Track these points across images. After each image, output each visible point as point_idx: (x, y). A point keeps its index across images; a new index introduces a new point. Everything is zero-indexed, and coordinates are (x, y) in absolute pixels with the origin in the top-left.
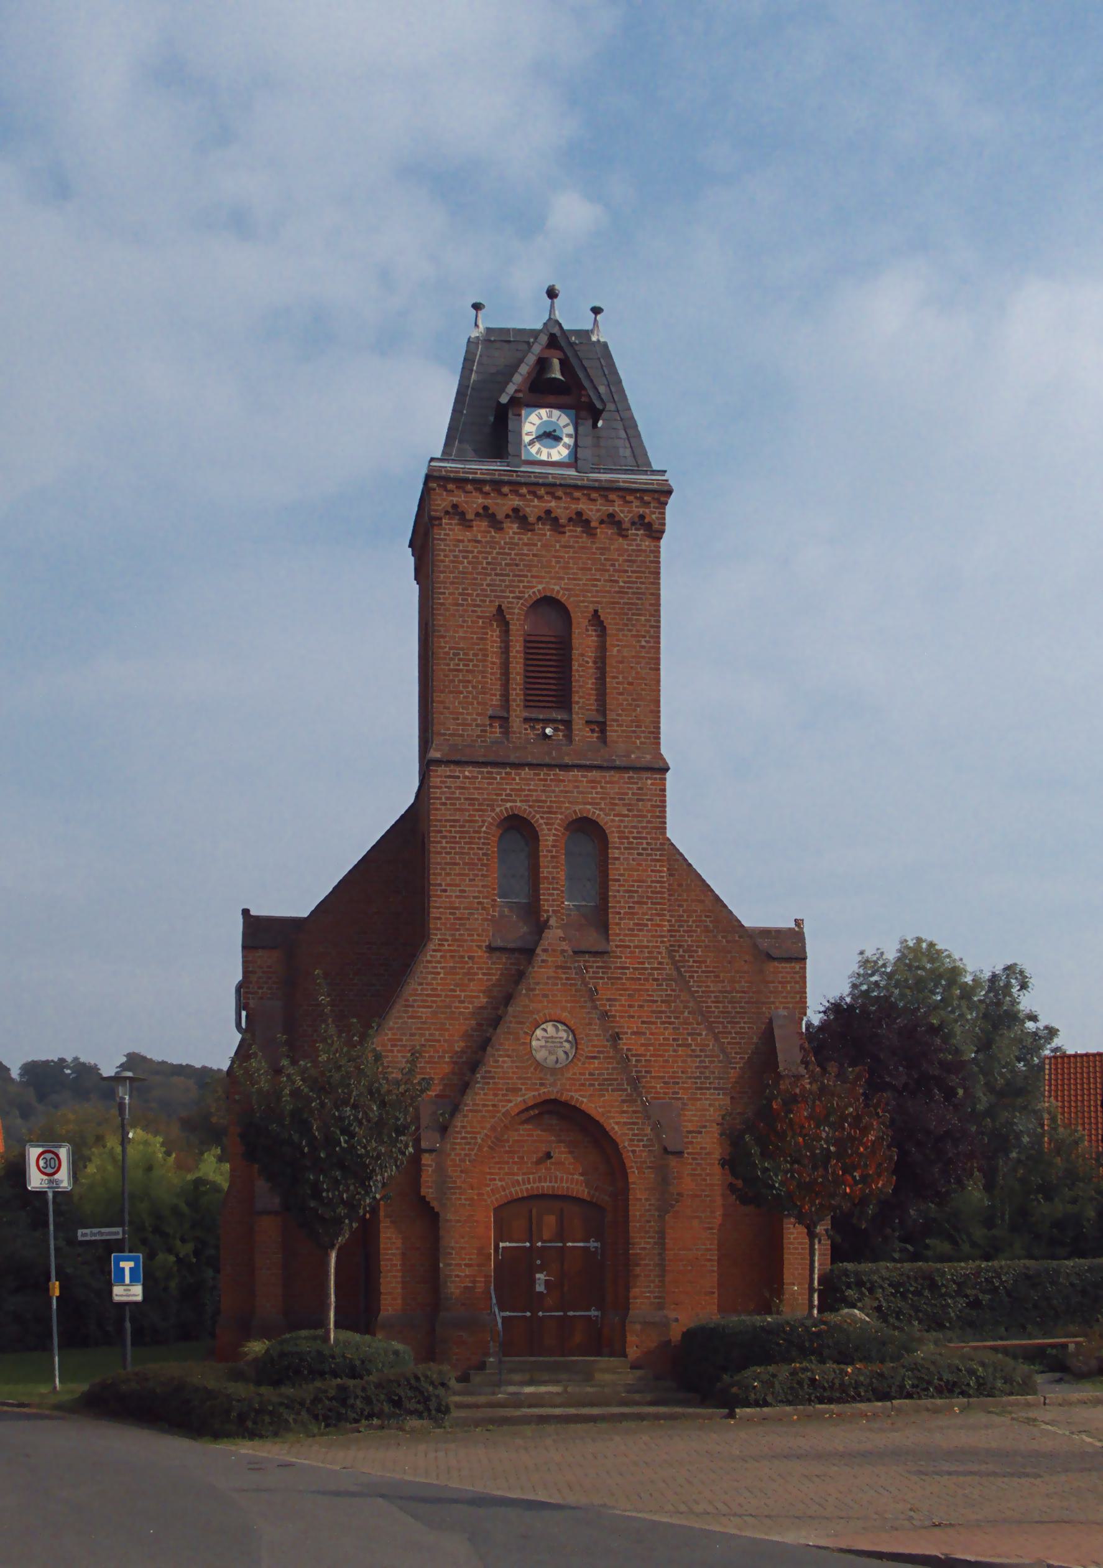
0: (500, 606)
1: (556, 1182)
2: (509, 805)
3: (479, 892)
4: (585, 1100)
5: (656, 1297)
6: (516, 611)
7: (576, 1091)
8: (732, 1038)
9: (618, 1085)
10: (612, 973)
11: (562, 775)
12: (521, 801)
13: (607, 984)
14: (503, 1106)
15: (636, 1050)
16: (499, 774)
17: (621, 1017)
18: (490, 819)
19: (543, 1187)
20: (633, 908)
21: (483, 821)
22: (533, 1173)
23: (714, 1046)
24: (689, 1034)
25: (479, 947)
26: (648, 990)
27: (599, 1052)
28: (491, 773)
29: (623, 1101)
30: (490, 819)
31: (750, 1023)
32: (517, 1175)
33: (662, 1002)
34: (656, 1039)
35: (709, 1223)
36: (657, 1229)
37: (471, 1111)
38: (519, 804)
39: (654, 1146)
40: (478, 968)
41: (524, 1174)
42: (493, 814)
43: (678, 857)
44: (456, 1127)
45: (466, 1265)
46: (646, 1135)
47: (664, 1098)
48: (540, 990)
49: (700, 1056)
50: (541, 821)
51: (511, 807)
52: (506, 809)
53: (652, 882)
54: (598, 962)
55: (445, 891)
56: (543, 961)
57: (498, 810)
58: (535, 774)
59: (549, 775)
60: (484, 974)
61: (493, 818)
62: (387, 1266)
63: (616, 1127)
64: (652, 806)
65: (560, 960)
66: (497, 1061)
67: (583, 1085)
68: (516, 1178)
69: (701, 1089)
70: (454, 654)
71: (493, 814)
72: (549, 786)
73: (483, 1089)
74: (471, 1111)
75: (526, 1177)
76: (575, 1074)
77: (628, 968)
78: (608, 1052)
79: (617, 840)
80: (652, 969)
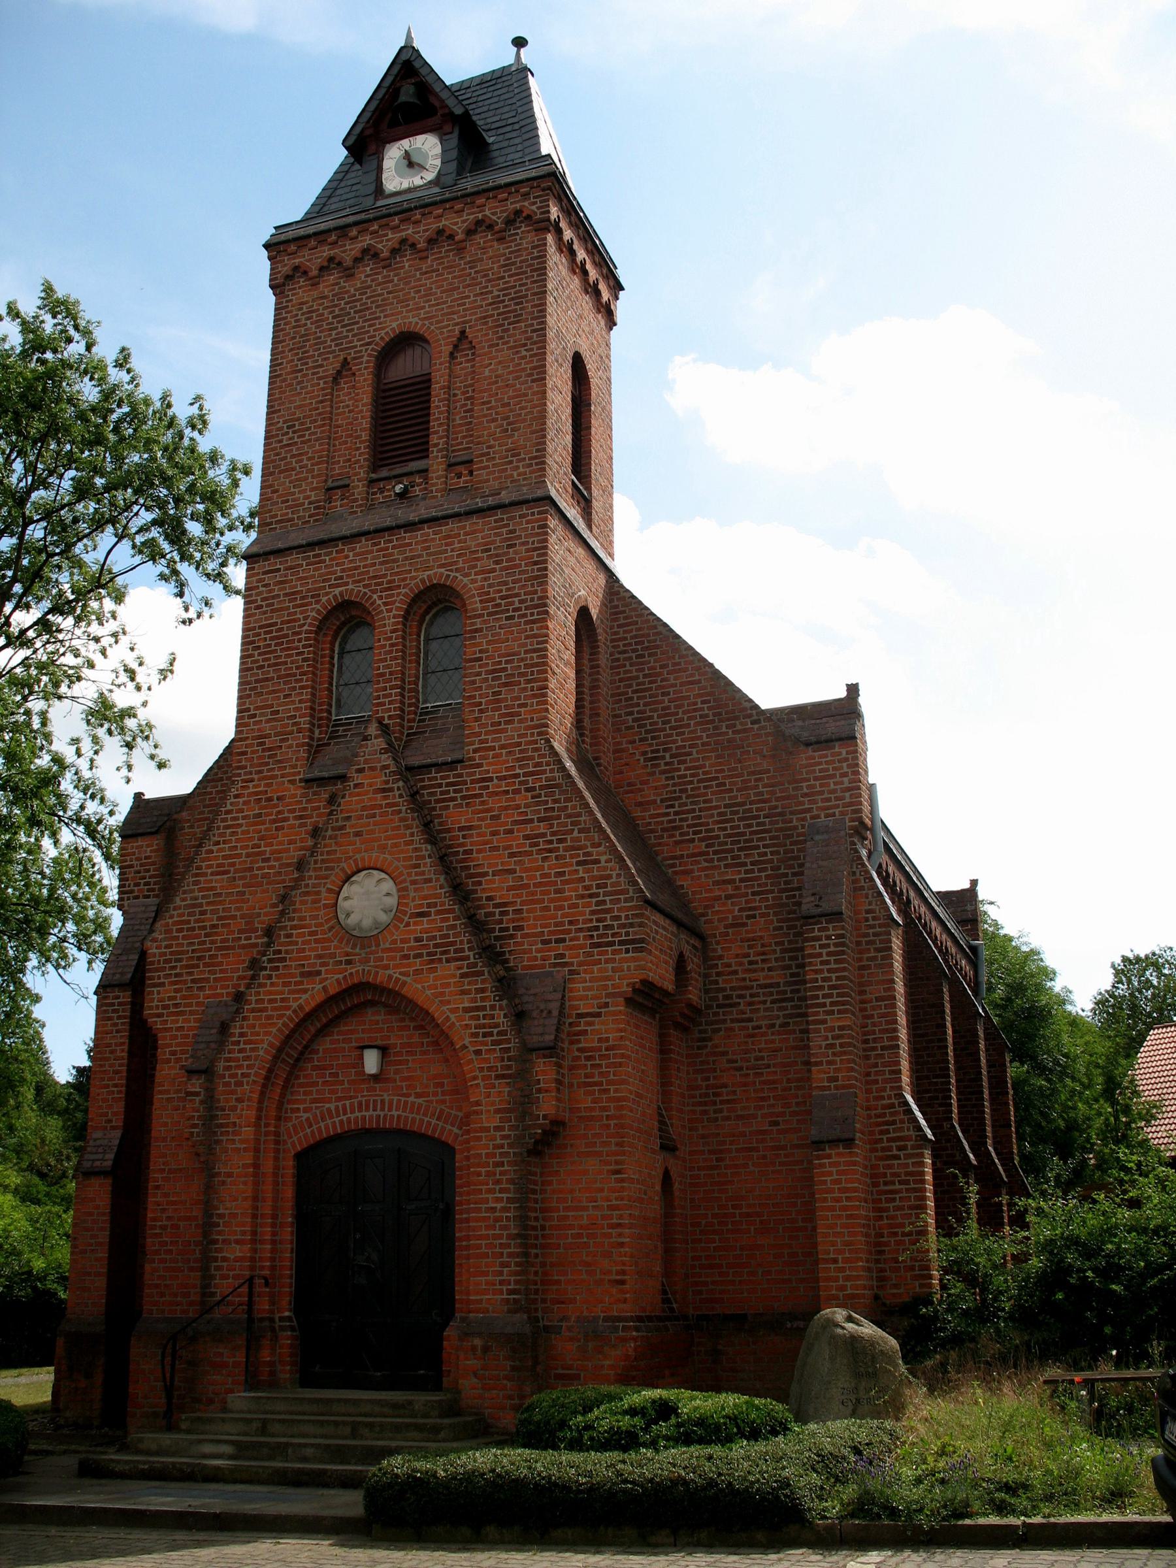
0: (346, 359)
1: (382, 1109)
2: (337, 591)
3: (296, 709)
4: (408, 979)
5: (510, 1292)
6: (365, 358)
7: (396, 967)
8: (746, 872)
9: (456, 951)
10: (468, 789)
11: (407, 536)
12: (355, 582)
13: (461, 806)
14: (296, 1000)
15: (501, 898)
16: (327, 556)
17: (479, 851)
18: (314, 614)
19: (364, 1118)
20: (499, 693)
22: (351, 1098)
23: (619, 875)
24: (579, 863)
25: (292, 782)
26: (518, 807)
27: (429, 905)
28: (319, 555)
29: (463, 976)
30: (314, 614)
31: (774, 845)
32: (329, 1101)
33: (540, 820)
34: (530, 878)
35: (617, 1163)
36: (512, 1176)
37: (253, 1010)
38: (350, 587)
39: (508, 1041)
41: (339, 1099)
42: (318, 607)
43: (660, 628)
44: (233, 1035)
45: (237, 1242)
46: (496, 1026)
47: (544, 966)
48: (352, 827)
49: (597, 895)
50: (379, 602)
51: (341, 594)
52: (335, 597)
53: (526, 652)
54: (448, 777)
55: (254, 716)
57: (324, 599)
58: (375, 544)
59: (391, 541)
60: (296, 818)
61: (318, 612)
63: (452, 1017)
64: (528, 551)
65: (379, 782)
67: (406, 957)
68: (327, 1105)
69: (599, 945)
70: (288, 427)
71: (318, 607)
72: (392, 554)
73: (270, 977)
74: (253, 1010)
75: (340, 1104)
76: (394, 942)
77: (491, 779)
78: (443, 904)
79: (478, 605)
80: (525, 775)
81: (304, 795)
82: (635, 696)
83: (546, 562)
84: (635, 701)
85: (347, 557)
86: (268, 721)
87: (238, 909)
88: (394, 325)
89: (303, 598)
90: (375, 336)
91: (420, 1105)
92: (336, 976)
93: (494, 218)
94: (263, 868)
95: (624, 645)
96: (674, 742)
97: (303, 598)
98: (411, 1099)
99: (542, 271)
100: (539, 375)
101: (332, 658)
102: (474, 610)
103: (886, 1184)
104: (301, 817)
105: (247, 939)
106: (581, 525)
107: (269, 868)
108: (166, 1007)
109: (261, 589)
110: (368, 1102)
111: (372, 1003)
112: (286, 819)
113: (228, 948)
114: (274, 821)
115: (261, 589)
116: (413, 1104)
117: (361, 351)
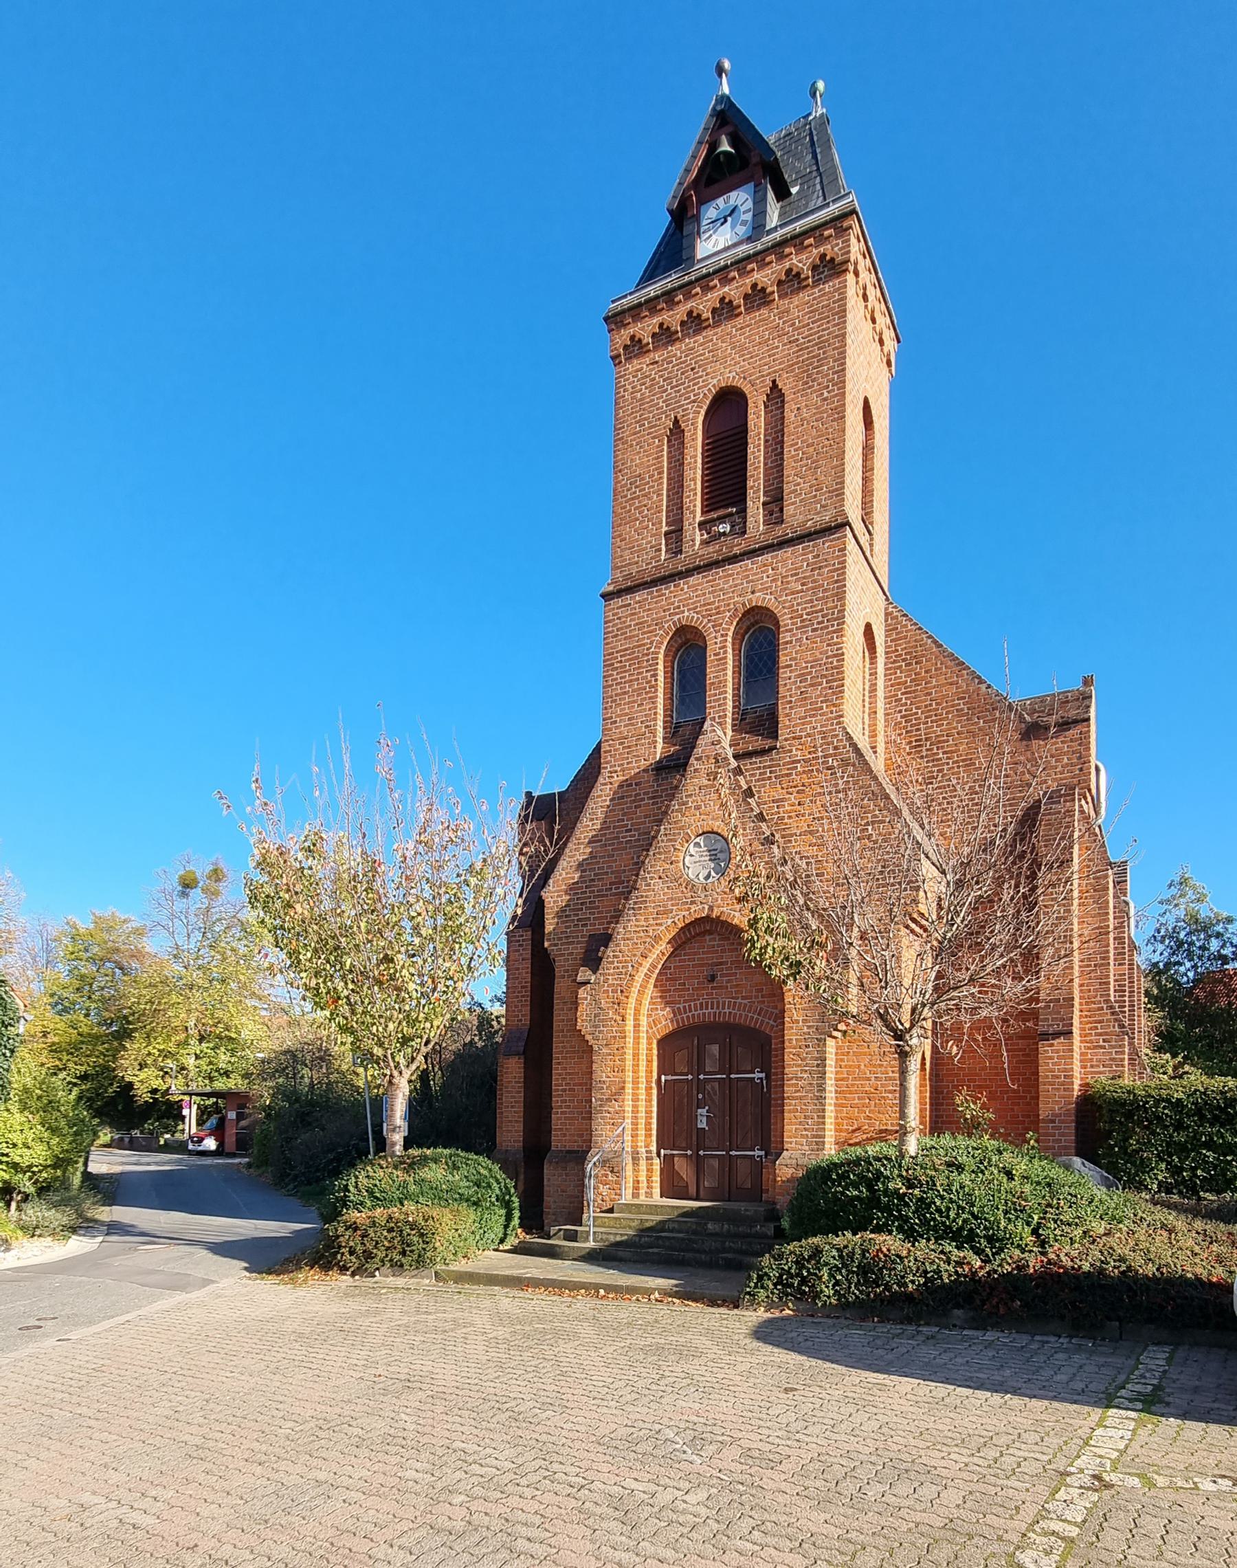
16: (668, 590)
17: (790, 817)
21: (652, 643)
22: (695, 1000)
40: (644, 794)
55: (616, 722)
56: (696, 770)
60: (649, 798)
62: (893, 1072)
66: (649, 885)
81: (657, 780)
82: (904, 697)
83: (844, 579)
84: (904, 701)
85: (682, 590)
86: (625, 726)
87: (609, 867)
88: (715, 381)
89: (649, 626)
90: (699, 394)
91: (745, 1005)
92: (684, 913)
93: (800, 265)
94: (626, 837)
95: (896, 656)
96: (935, 732)
97: (649, 626)
98: (739, 1000)
99: (843, 312)
100: (839, 414)
101: (673, 674)
102: (786, 625)
103: (1092, 1066)
104: (653, 798)
105: (616, 889)
106: (868, 554)
107: (630, 836)
108: (560, 939)
109: (617, 621)
110: (707, 1004)
111: (710, 932)
112: (643, 799)
113: (603, 896)
114: (634, 801)
115: (617, 621)
116: (740, 1004)
117: (687, 409)
